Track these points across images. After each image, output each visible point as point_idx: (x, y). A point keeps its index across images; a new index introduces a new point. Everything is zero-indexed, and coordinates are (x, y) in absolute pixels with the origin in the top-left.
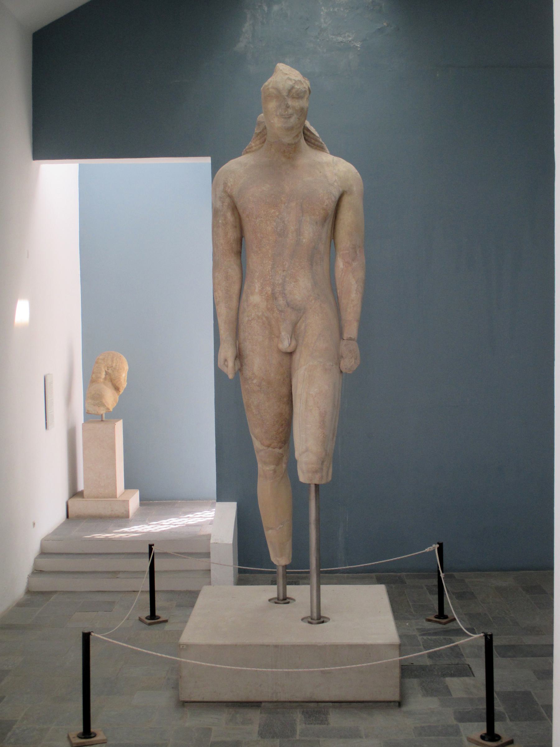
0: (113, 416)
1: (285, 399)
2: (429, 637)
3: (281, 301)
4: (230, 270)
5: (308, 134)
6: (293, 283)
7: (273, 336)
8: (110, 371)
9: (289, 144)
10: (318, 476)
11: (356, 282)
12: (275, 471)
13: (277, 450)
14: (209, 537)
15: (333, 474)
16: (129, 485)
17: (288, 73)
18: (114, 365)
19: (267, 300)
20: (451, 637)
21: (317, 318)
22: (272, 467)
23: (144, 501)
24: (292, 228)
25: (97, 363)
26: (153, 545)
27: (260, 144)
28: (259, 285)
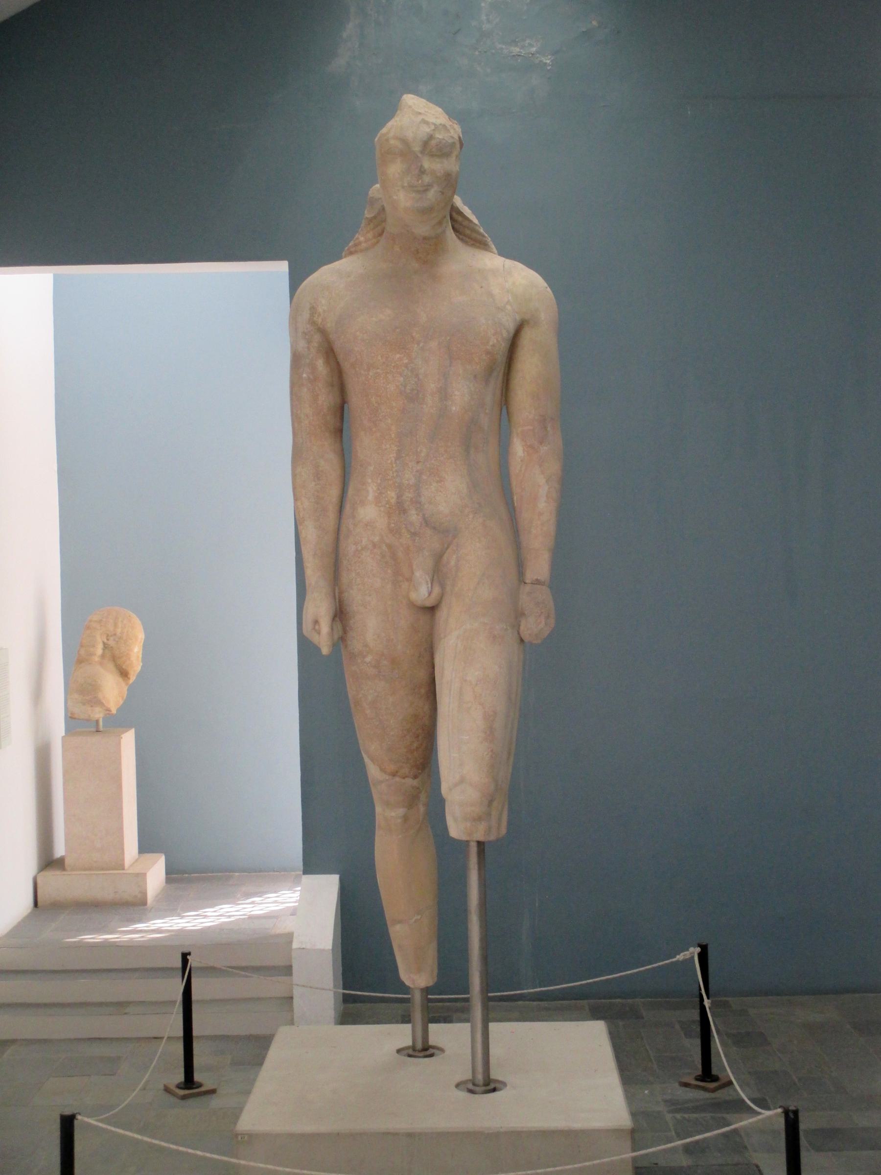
2: (686, 1116)
3: (414, 516)
5: (460, 219)
8: (111, 643)
9: (425, 238)
11: (547, 481)
12: (405, 818)
13: (410, 782)
16: (146, 846)
17: (422, 111)
18: (119, 630)
20: (725, 1115)
22: (401, 811)
23: (173, 874)
24: (432, 385)
25: (88, 628)
26: (189, 954)
27: (374, 237)
28: (375, 488)
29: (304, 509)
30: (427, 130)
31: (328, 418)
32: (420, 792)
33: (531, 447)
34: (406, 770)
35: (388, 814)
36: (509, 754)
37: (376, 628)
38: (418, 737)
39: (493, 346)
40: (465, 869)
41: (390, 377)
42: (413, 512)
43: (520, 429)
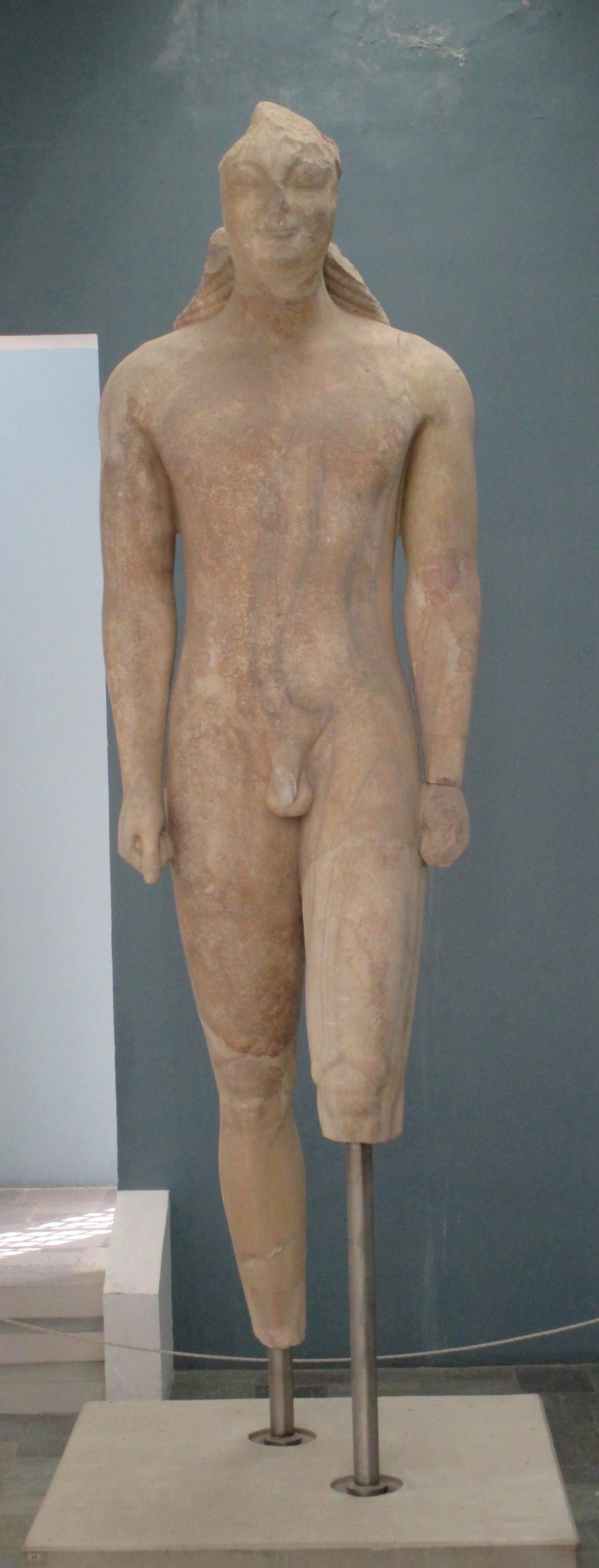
1: (286, 934)
3: (273, 691)
5: (337, 275)
7: (254, 777)
11: (459, 642)
12: (261, 1112)
13: (267, 1061)
14: (99, 1277)
17: (284, 125)
22: (255, 1102)
24: (299, 508)
28: (219, 651)
30: (290, 151)
34: (261, 1045)
35: (236, 1106)
36: (406, 1021)
38: (278, 997)
41: (239, 495)
43: (421, 569)
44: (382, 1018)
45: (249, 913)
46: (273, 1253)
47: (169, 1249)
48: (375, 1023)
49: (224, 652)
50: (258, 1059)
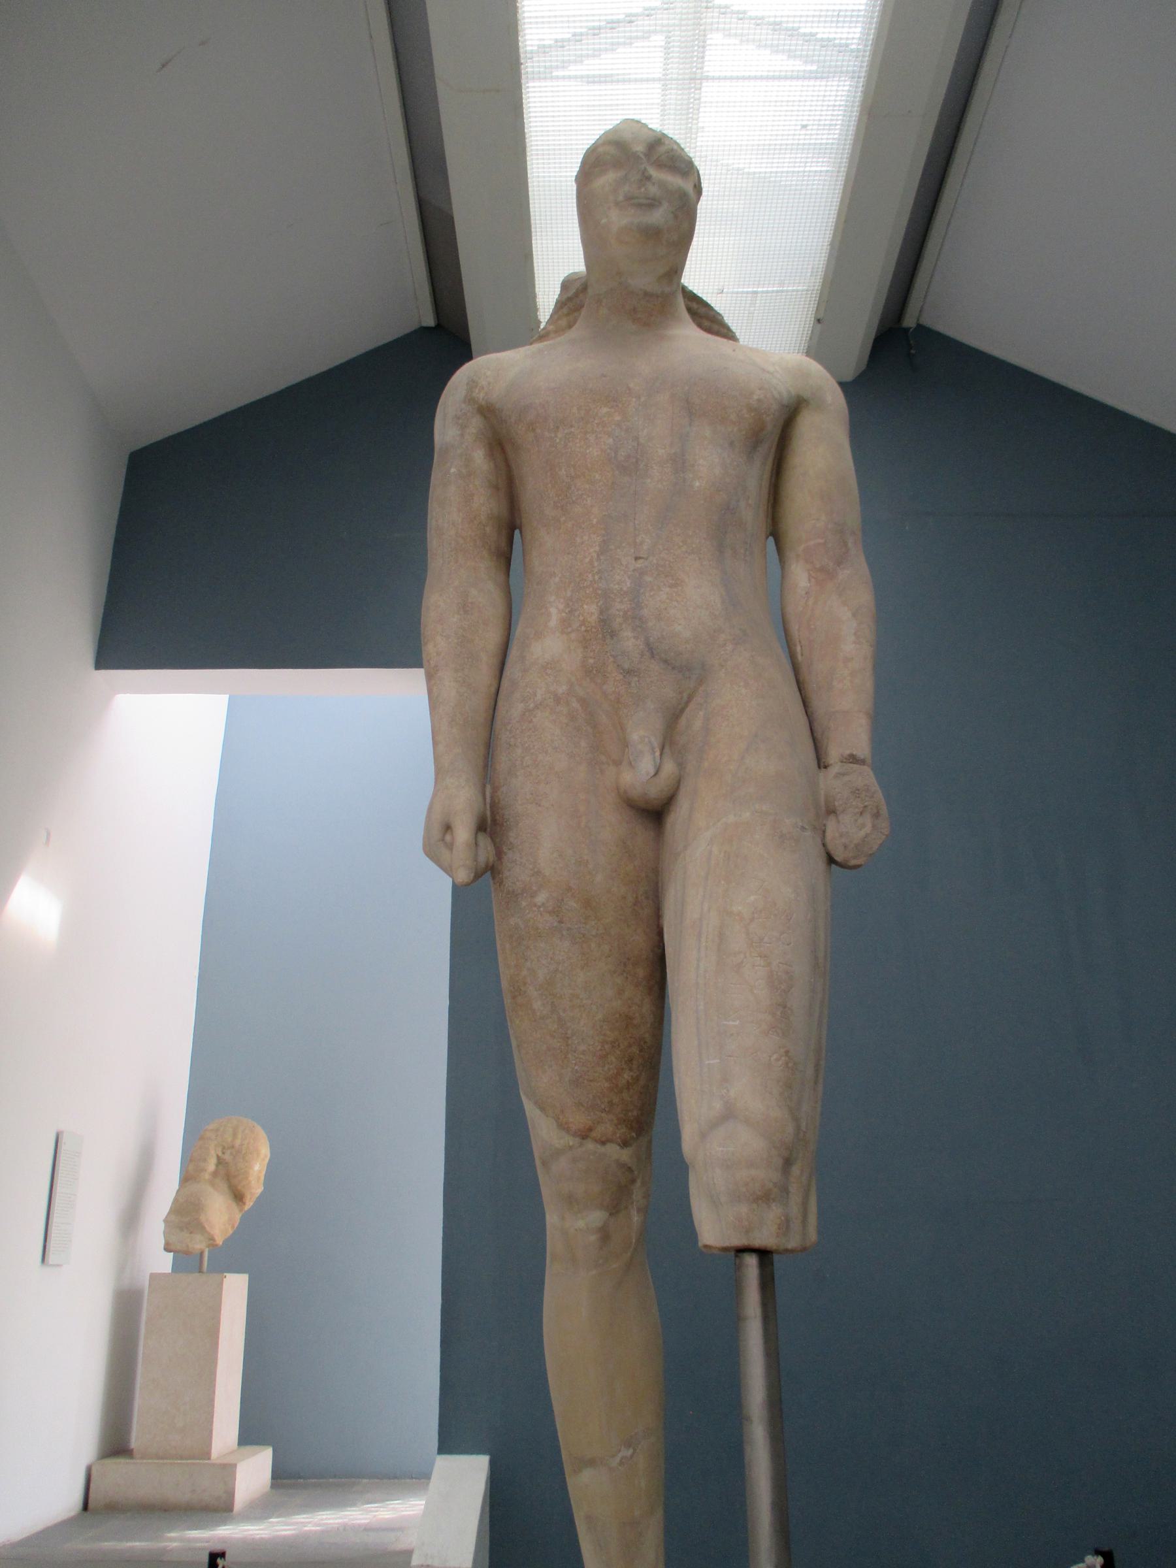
0: (227, 1258)
1: (641, 972)
3: (630, 641)
4: (474, 592)
6: (668, 589)
7: (603, 758)
8: (227, 1157)
9: (646, 294)
10: (773, 1214)
11: (854, 615)
12: (605, 1235)
13: (614, 1152)
14: (409, 1553)
15: (821, 1213)
16: (249, 1436)
18: (238, 1142)
19: (585, 643)
21: (743, 691)
22: (596, 1217)
23: (281, 1476)
24: (661, 452)
25: (202, 1138)
28: (561, 607)
29: (438, 654)
30: (755, 1206)
31: (488, 529)
32: (633, 1181)
33: (822, 569)
34: (606, 1128)
35: (570, 1226)
36: (817, 1071)
37: (560, 837)
38: (631, 1060)
39: (759, 400)
40: (736, 1320)
41: (592, 438)
42: (627, 633)
43: (803, 546)
44: (787, 1052)
45: (594, 933)
46: (618, 1459)
47: (487, 1520)
48: (777, 1060)
49: (567, 605)
50: (601, 1149)
